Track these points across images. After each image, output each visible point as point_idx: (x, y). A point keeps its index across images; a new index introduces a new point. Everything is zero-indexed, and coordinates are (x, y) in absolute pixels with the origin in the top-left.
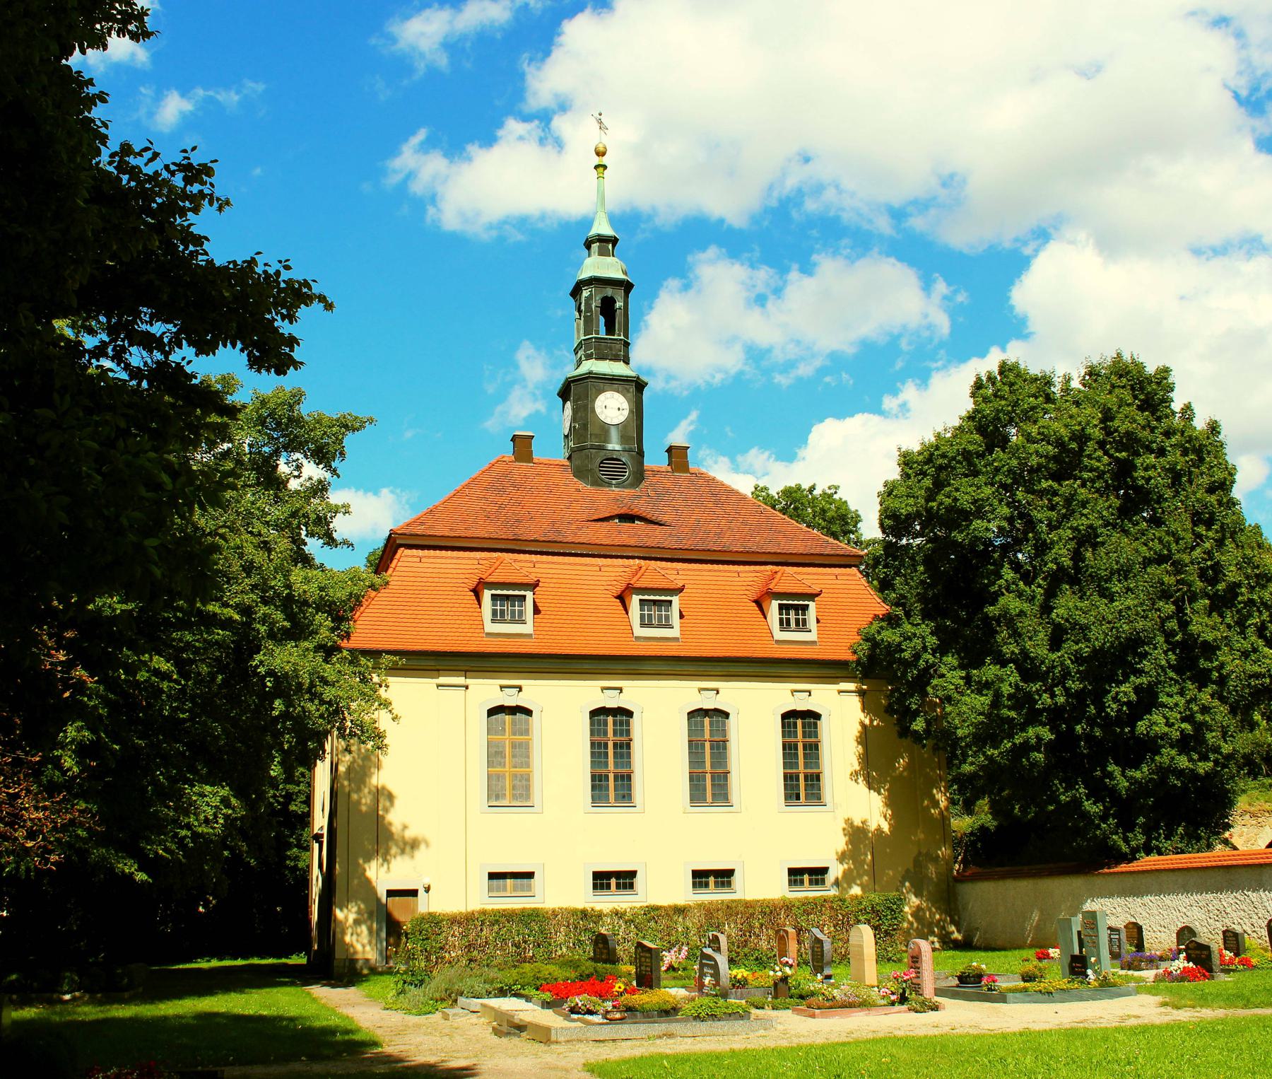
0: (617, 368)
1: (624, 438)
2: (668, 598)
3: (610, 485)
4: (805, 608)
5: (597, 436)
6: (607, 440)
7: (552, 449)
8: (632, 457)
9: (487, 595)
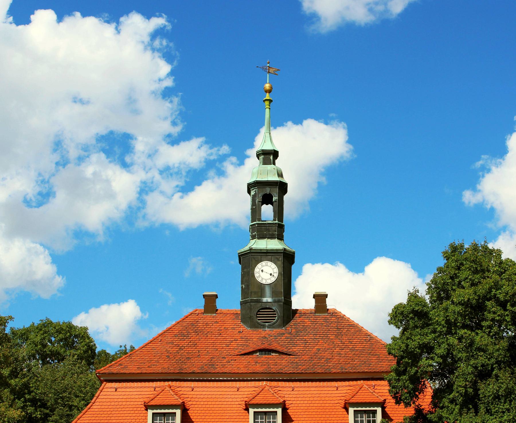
0: (274, 244)
1: (274, 294)
2: (275, 410)
3: (264, 327)
4: (375, 412)
5: (255, 293)
6: (263, 295)
7: (231, 301)
8: (280, 305)
9: (351, 410)
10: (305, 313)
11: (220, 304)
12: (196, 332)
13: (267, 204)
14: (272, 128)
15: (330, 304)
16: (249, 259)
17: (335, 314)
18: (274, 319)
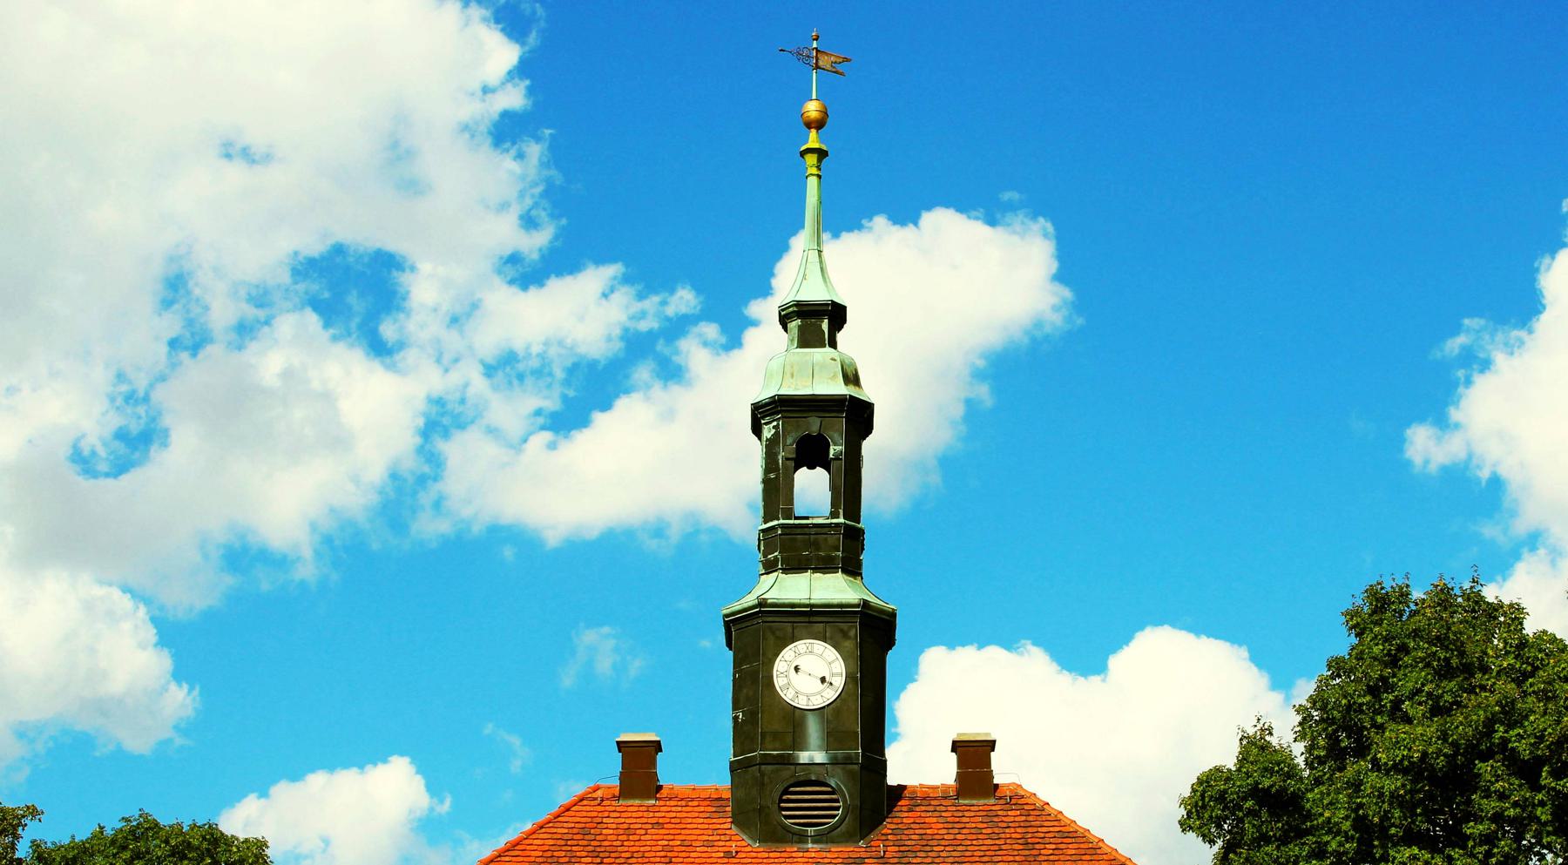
3: (802, 838)
6: (799, 743)
7: (700, 760)
10: (926, 798)
11: (667, 771)
15: (1003, 769)
16: (756, 635)
17: (1017, 800)
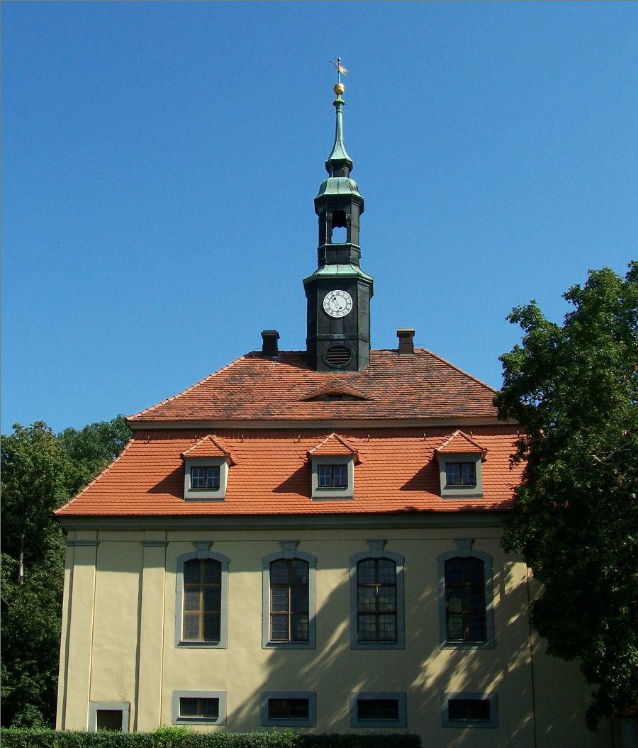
3: (335, 369)
12: (251, 375)
13: (340, 227)
14: (532, 631)
18: (348, 360)
